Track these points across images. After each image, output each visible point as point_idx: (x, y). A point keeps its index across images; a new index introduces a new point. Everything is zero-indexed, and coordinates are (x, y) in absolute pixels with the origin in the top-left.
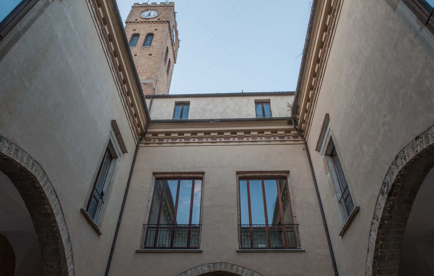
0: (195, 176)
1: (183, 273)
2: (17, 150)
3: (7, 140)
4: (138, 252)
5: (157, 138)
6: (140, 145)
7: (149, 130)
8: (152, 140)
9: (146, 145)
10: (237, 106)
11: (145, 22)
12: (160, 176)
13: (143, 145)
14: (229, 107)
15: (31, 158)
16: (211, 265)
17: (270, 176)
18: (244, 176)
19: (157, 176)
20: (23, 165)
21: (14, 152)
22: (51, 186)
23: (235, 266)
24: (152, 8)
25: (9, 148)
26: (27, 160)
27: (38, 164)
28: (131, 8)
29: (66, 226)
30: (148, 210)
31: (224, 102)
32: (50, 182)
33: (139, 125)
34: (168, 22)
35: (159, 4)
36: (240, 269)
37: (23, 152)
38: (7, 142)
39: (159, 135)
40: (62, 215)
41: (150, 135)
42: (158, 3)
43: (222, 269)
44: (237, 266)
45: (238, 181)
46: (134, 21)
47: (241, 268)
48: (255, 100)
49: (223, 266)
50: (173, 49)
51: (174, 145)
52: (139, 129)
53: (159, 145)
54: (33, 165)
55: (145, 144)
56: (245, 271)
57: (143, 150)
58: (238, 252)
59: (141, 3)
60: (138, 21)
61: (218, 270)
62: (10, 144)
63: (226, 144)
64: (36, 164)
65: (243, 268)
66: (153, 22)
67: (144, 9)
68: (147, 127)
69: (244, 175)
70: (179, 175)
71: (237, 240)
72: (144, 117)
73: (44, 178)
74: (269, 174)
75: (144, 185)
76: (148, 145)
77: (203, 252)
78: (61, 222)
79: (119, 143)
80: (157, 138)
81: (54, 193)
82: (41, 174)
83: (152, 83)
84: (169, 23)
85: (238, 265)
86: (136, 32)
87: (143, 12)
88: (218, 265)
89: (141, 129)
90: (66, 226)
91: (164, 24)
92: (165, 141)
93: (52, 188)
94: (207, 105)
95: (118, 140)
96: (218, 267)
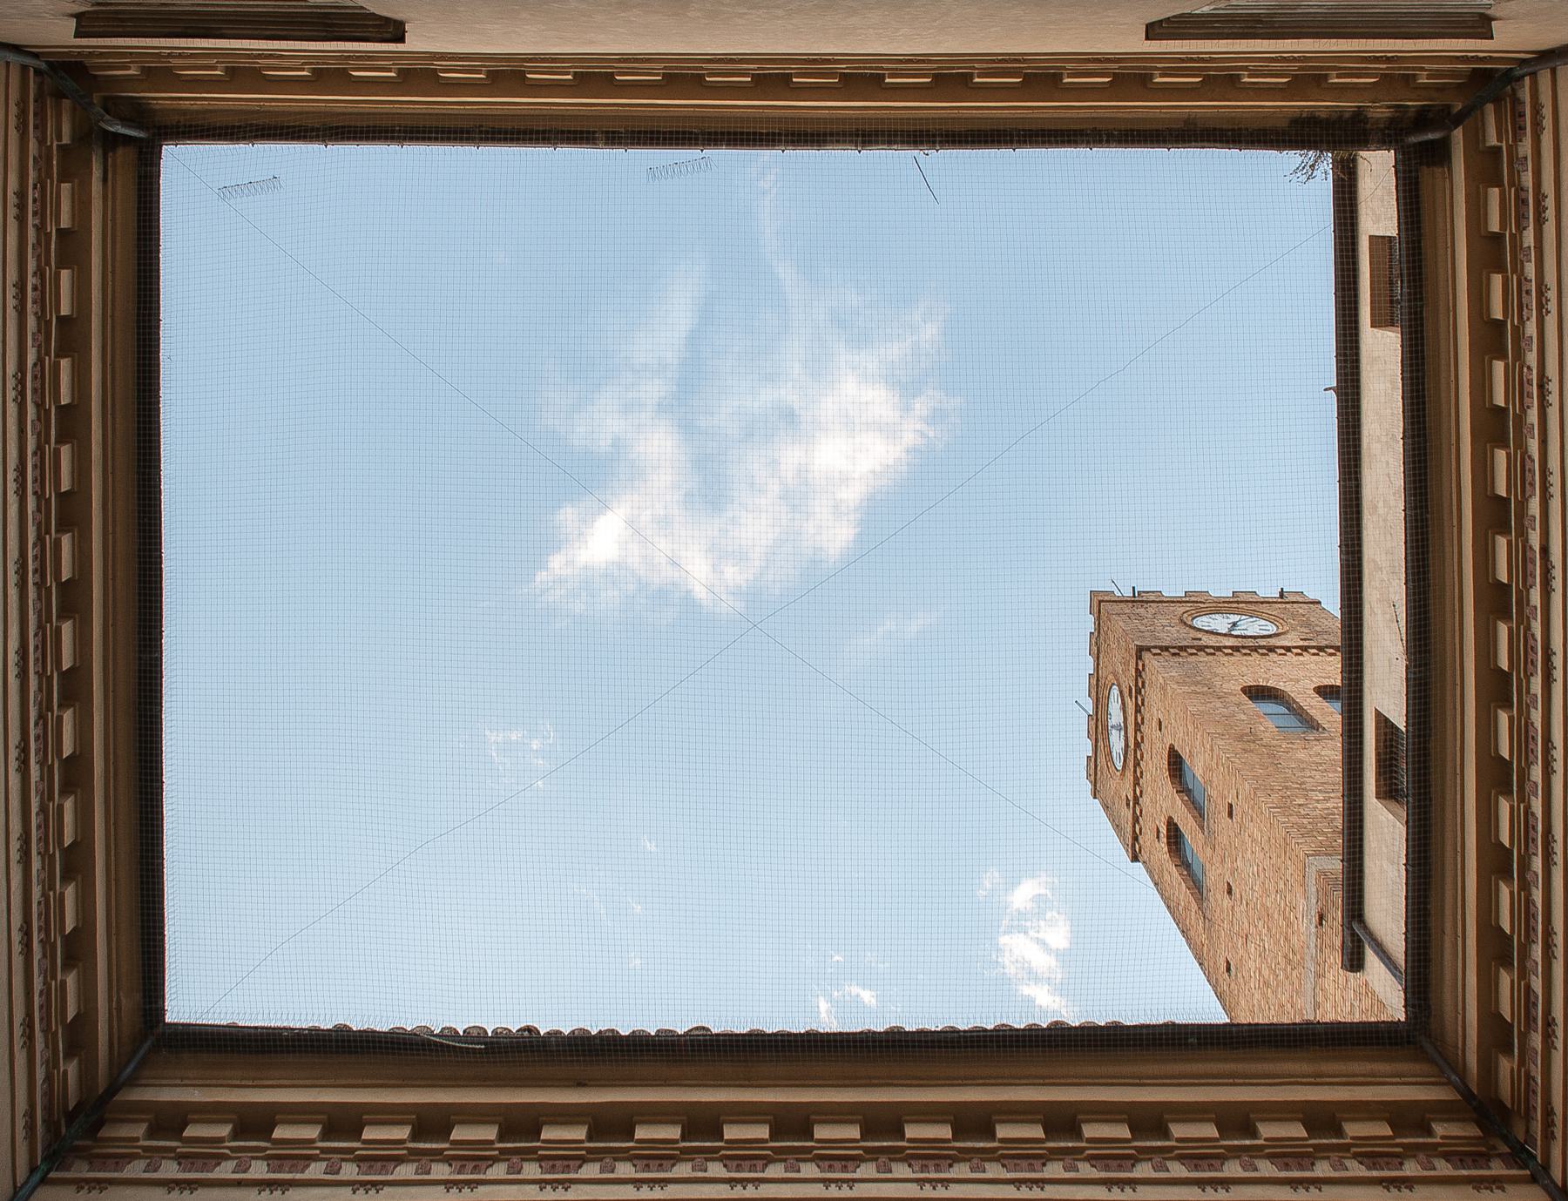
33: (1408, 1119)
34: (1140, 650)
68: (1444, 1063)
72: (1368, 1067)
84: (1148, 649)
86: (1164, 830)
89: (1444, 1111)
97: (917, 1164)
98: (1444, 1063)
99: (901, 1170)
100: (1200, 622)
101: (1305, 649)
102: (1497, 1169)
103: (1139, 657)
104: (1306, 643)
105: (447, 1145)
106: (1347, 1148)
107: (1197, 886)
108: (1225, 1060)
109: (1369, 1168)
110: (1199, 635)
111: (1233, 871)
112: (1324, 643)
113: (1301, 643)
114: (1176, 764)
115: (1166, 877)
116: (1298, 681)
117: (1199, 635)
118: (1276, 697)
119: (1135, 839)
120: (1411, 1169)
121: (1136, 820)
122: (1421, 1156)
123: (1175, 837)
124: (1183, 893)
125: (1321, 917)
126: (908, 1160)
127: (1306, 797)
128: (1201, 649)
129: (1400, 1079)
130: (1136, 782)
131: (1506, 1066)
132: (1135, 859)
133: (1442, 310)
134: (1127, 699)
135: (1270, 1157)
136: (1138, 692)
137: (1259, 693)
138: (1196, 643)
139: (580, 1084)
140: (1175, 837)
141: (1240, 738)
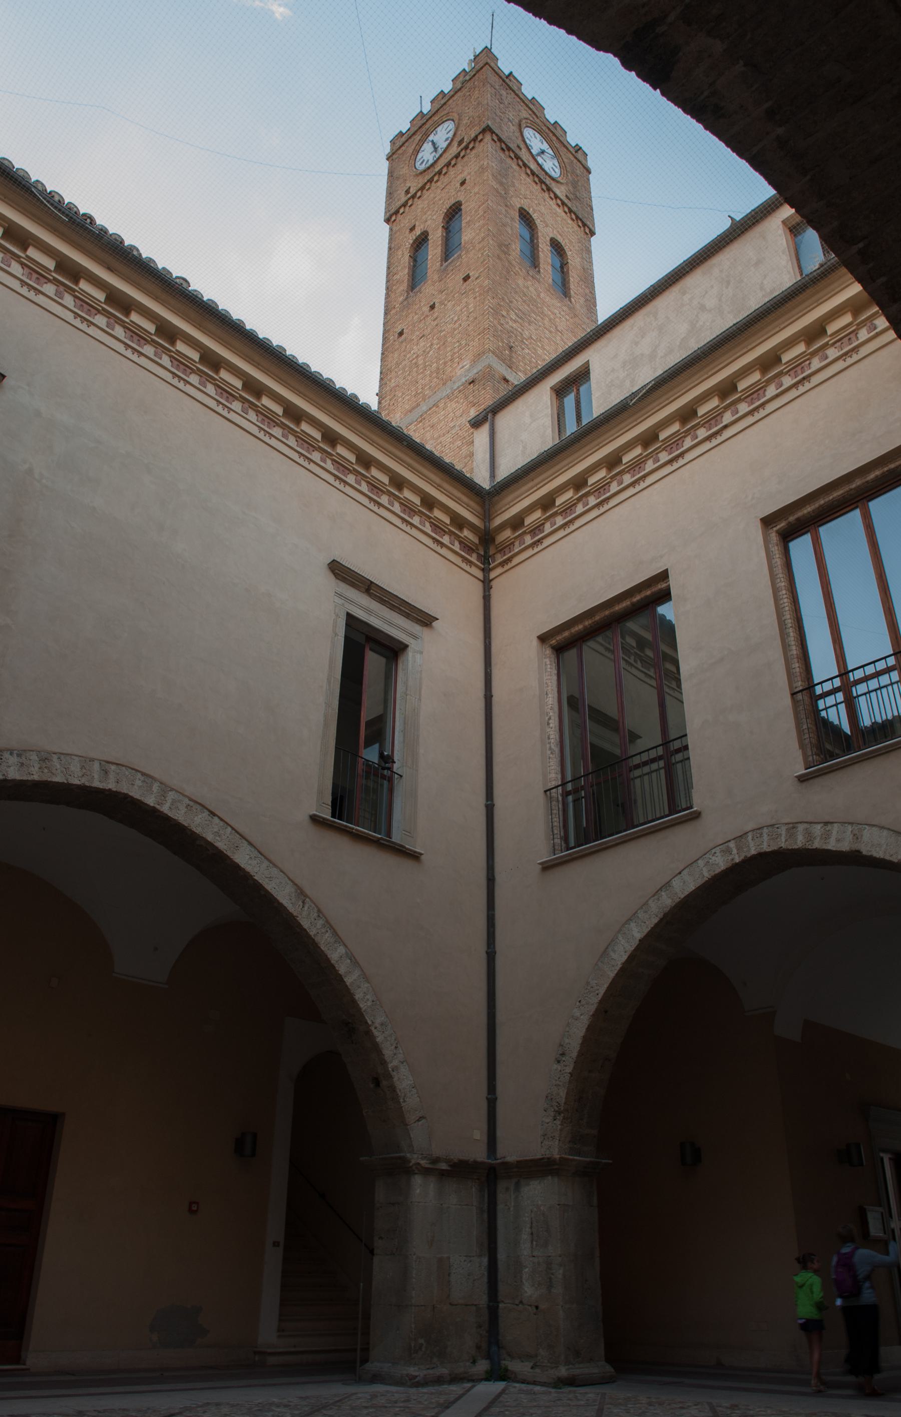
0: (648, 593)
1: (661, 889)
2: (43, 760)
3: (8, 750)
4: (547, 867)
5: (524, 533)
6: (493, 575)
7: (498, 521)
8: (517, 543)
9: (506, 567)
10: (728, 283)
11: (431, 181)
12: (559, 638)
13: (499, 571)
14: (702, 308)
15: (92, 760)
16: (732, 845)
17: (883, 475)
18: (795, 522)
19: (553, 642)
20: (79, 783)
21: (37, 766)
22: (181, 797)
23: (801, 827)
24: (436, 118)
25: (22, 764)
26: (82, 767)
27: (117, 764)
28: (386, 164)
29: (275, 866)
30: (550, 749)
31: (686, 298)
32: (172, 789)
33: (459, 522)
34: (487, 129)
35: (451, 87)
36: (818, 829)
37: (62, 757)
38: (11, 754)
39: (528, 521)
40: (249, 847)
41: (507, 534)
42: (448, 87)
43: (765, 848)
44: (806, 825)
45: (776, 551)
46: (404, 199)
47: (819, 827)
48: (784, 222)
49: (765, 837)
50: (556, 197)
51: (572, 528)
52: (466, 533)
53: (536, 550)
54: (106, 772)
55: (502, 564)
56: (834, 832)
57: (506, 584)
58: (802, 779)
59: (405, 127)
60: (412, 191)
61: (753, 852)
62: (19, 755)
63: (715, 442)
64: (113, 767)
65: (826, 823)
66: (448, 165)
67: (418, 137)
68: (487, 515)
69: (792, 519)
70: (607, 613)
71: (796, 745)
72: (459, 494)
73: (151, 787)
74: (878, 473)
75: (530, 682)
76: (510, 565)
77: (703, 815)
78: (254, 862)
79: (393, 608)
80: (524, 533)
81: (199, 807)
82: (138, 783)
83: (490, 366)
84: (493, 132)
85: (810, 819)
86: (418, 232)
87: (417, 151)
88: (750, 837)
89: (473, 527)
90: (275, 866)
91: (480, 147)
92: (548, 528)
93: (187, 801)
94: (637, 344)
95: (382, 601)
96: (752, 844)
97: (261, 417)
98: (487, 515)
99: (252, 416)
100: (529, 133)
101: (563, 203)
102: (473, 558)
103: (483, 131)
104: (566, 201)
105: (23, 255)
106: (430, 518)
107: (415, 280)
108: (411, 458)
109: (432, 531)
110: (522, 146)
111: (442, 303)
112: (574, 209)
113: (564, 198)
114: (454, 211)
115: (400, 253)
116: (547, 226)
117: (522, 146)
118: (531, 227)
119: (397, 212)
120: (446, 540)
121: (404, 205)
122: (453, 537)
123: (421, 241)
124: (403, 274)
125: (473, 382)
126: (258, 412)
127: (508, 311)
128: (518, 157)
129: (467, 507)
130: (422, 188)
131: (507, 534)
132: (387, 221)
133: (814, 299)
134: (455, 144)
135: (401, 503)
136: (466, 148)
137: (525, 217)
138: (517, 151)
139: (110, 269)
140: (421, 241)
141: (500, 246)
